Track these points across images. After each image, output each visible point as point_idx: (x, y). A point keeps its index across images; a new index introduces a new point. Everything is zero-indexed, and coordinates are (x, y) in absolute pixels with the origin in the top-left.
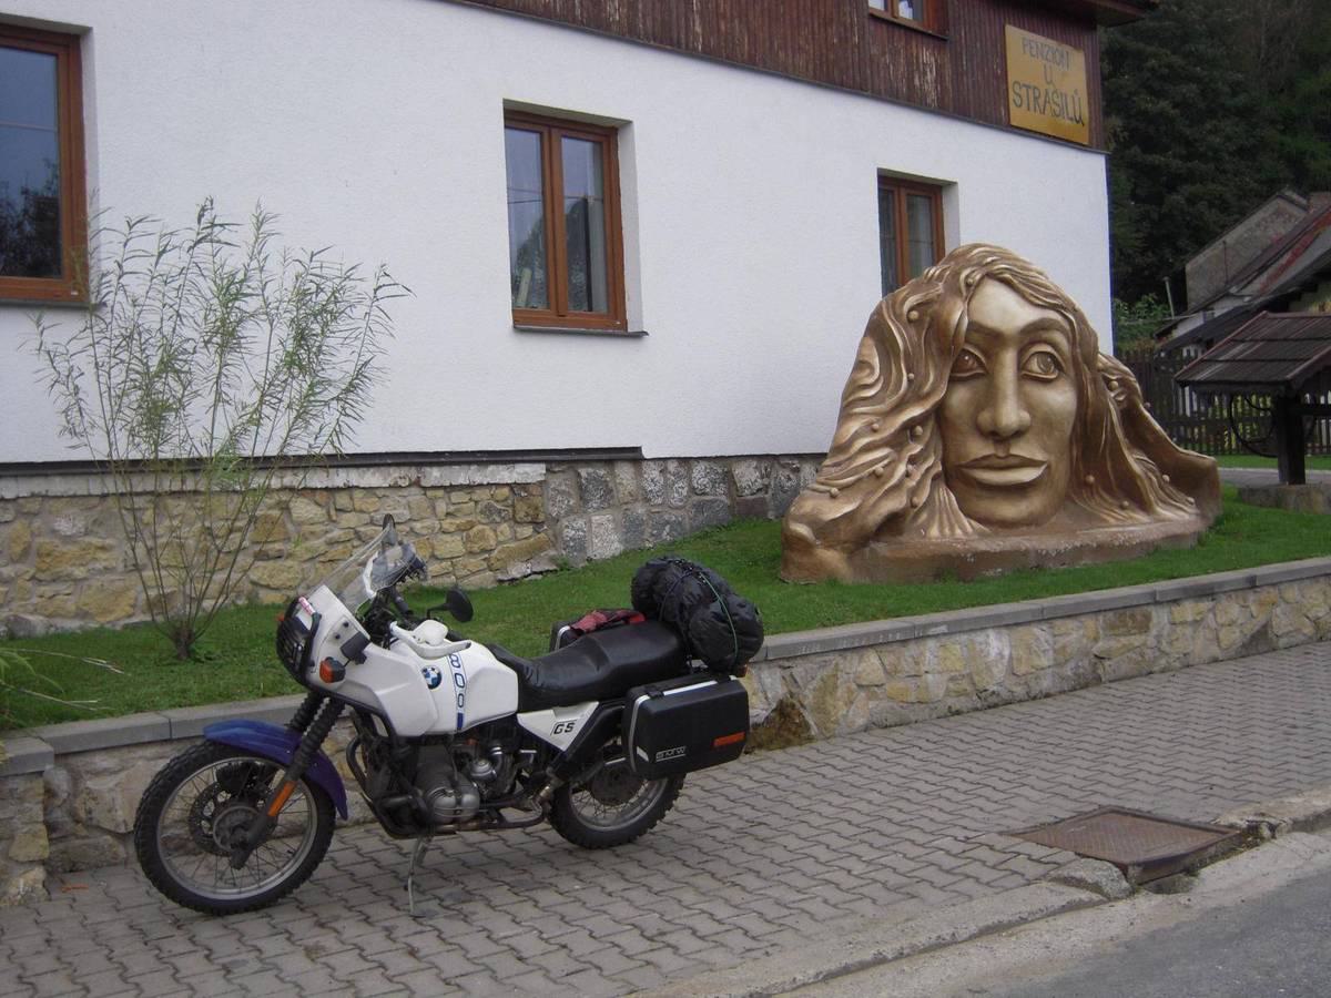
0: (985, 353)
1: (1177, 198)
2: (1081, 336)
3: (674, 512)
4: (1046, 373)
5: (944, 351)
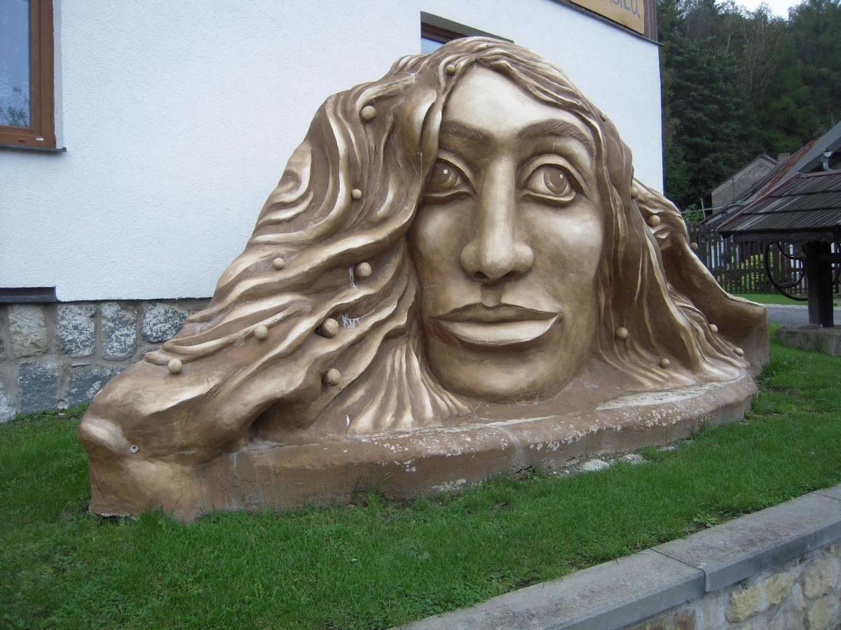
0: (469, 163)
1: (708, 160)
2: (609, 150)
3: (110, 365)
4: (557, 193)
5: (412, 162)
